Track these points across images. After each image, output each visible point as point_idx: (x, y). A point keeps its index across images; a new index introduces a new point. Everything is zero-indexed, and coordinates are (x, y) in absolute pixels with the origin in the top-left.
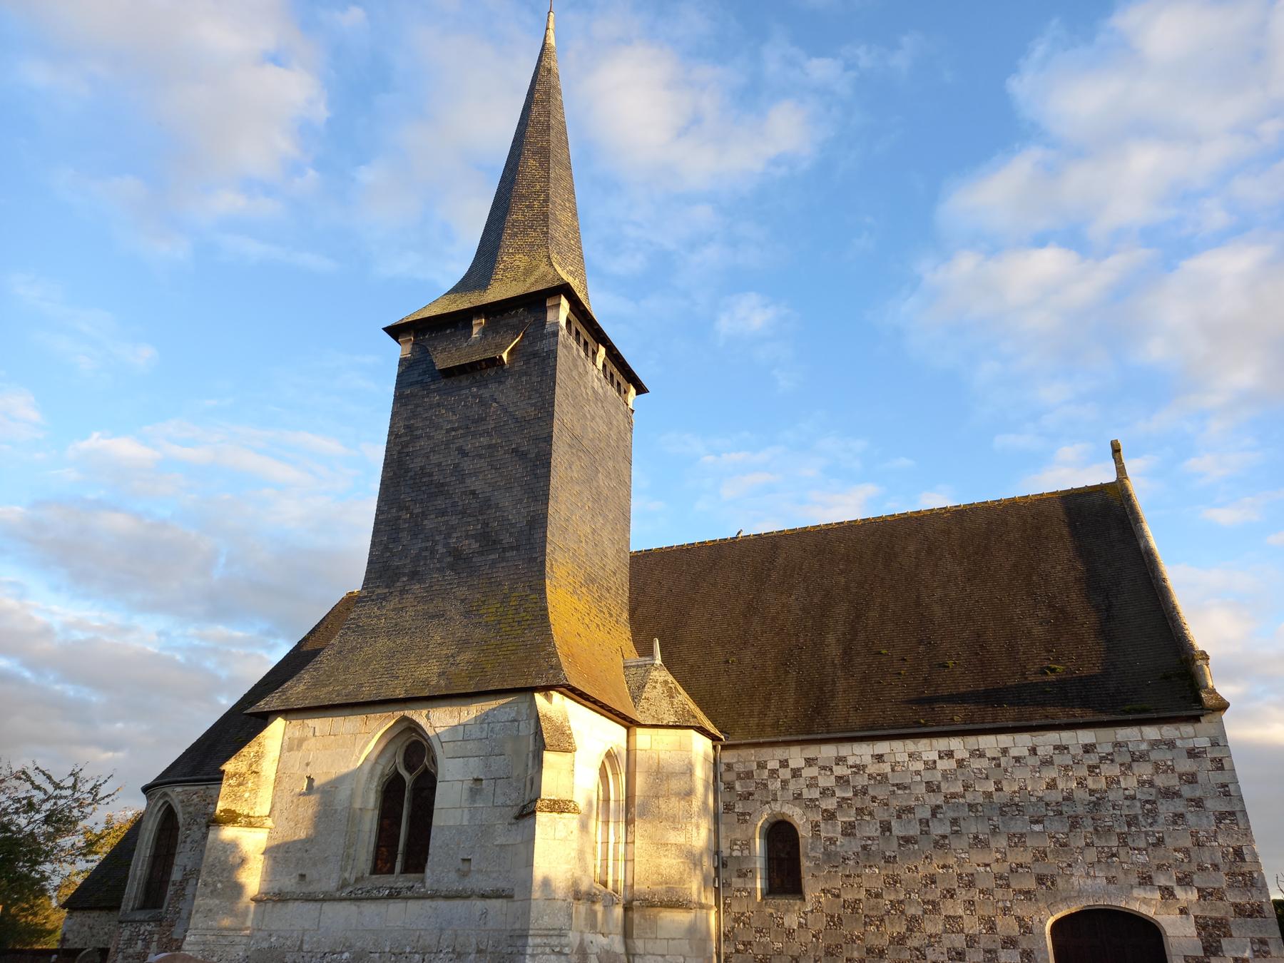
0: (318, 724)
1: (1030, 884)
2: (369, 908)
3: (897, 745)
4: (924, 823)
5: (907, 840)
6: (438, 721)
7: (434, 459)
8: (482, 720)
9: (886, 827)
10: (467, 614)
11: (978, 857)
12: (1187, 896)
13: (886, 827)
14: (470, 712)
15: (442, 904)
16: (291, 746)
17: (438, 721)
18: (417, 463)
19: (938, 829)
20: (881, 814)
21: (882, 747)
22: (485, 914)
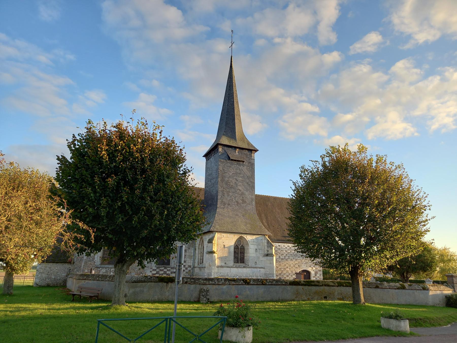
0: (225, 235)
1: (297, 266)
2: (239, 269)
3: (282, 244)
4: (285, 256)
5: (282, 259)
6: (249, 238)
7: (231, 179)
8: (256, 239)
9: (280, 257)
10: (243, 216)
11: (291, 262)
12: (314, 268)
13: (280, 257)
14: (254, 237)
15: (253, 269)
16: (219, 238)
17: (249, 238)
18: (226, 179)
19: (287, 258)
20: (279, 255)
21: (280, 244)
22: (260, 271)
